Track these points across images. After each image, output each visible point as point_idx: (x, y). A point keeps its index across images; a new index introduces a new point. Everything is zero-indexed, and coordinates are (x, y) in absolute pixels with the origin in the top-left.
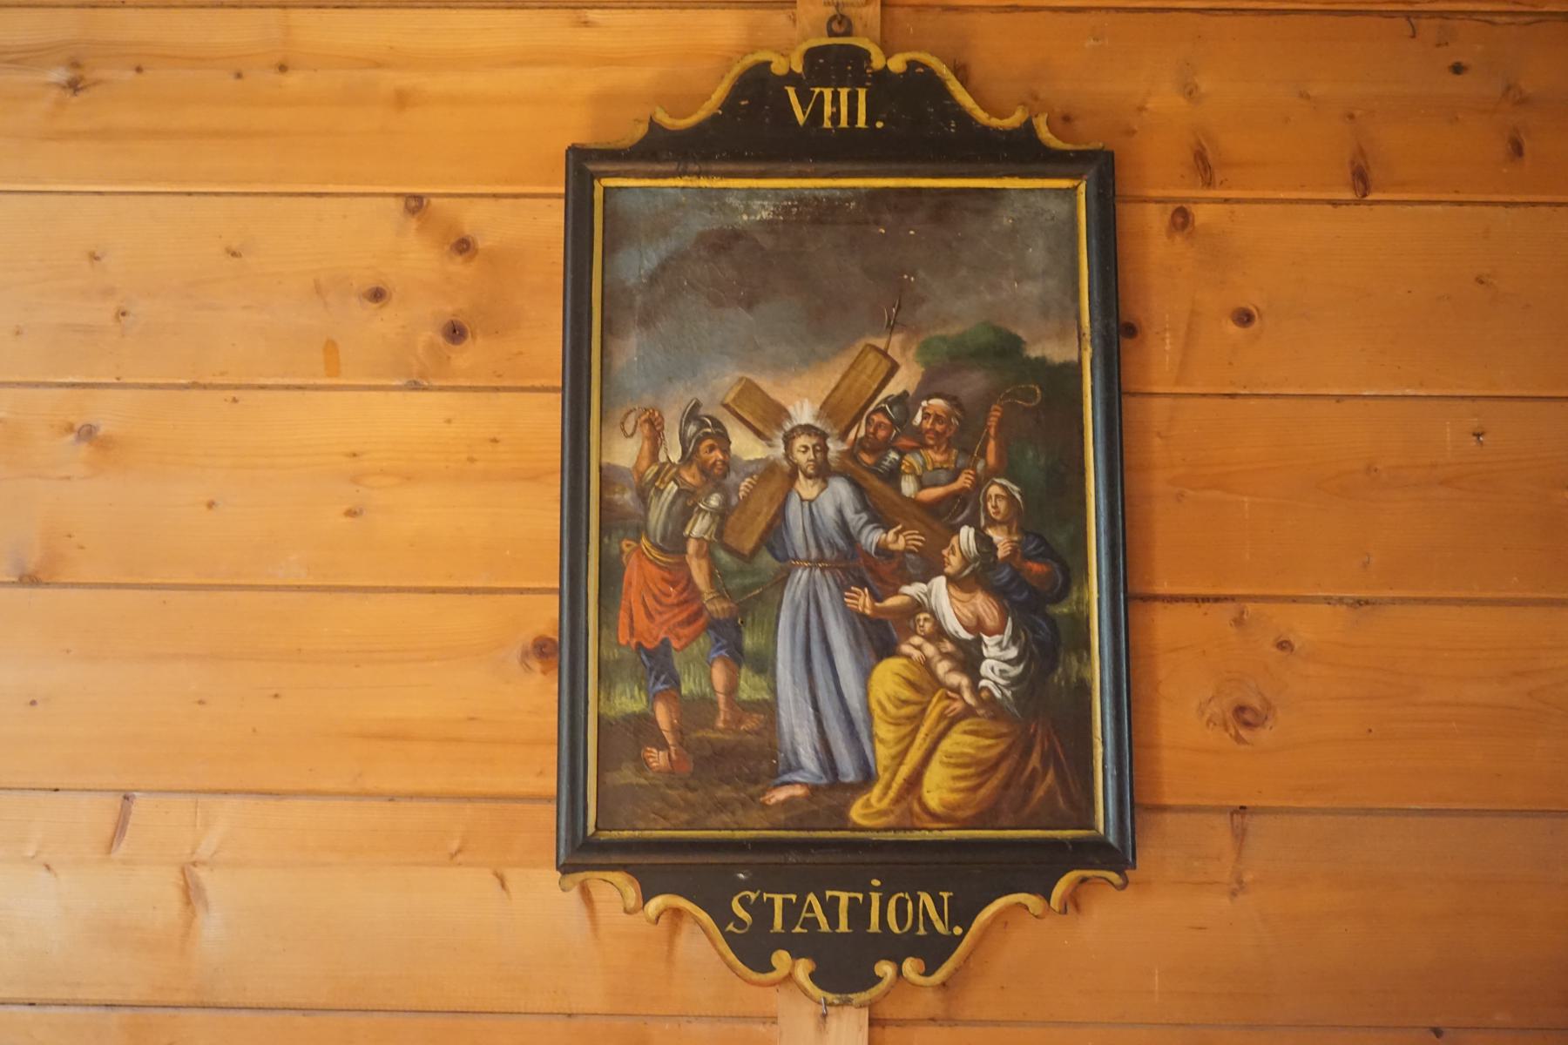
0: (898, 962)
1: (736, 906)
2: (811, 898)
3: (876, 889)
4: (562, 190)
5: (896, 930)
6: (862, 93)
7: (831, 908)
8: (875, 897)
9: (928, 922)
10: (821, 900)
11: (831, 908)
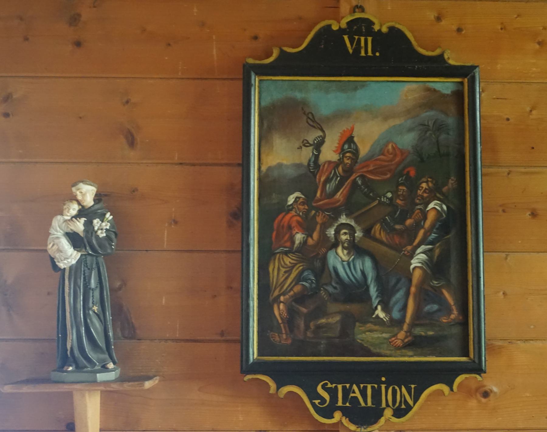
0: (380, 31)
1: (319, 389)
2: (355, 387)
3: (383, 383)
4: (241, 77)
5: (396, 387)
6: (370, 39)
7: (363, 393)
8: (383, 386)
9: (406, 401)
10: (359, 387)
11: (363, 393)
